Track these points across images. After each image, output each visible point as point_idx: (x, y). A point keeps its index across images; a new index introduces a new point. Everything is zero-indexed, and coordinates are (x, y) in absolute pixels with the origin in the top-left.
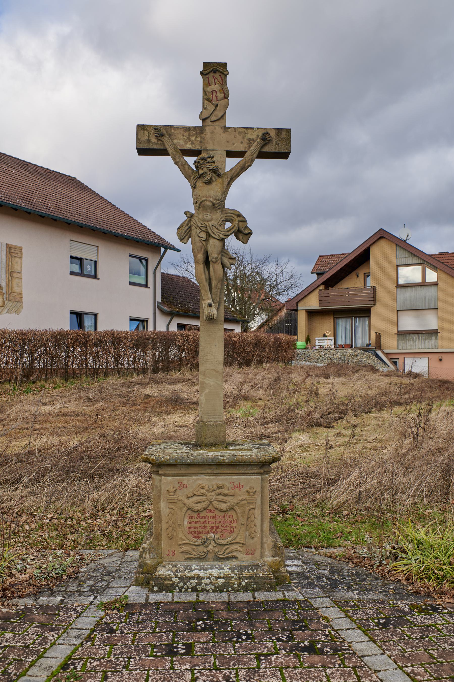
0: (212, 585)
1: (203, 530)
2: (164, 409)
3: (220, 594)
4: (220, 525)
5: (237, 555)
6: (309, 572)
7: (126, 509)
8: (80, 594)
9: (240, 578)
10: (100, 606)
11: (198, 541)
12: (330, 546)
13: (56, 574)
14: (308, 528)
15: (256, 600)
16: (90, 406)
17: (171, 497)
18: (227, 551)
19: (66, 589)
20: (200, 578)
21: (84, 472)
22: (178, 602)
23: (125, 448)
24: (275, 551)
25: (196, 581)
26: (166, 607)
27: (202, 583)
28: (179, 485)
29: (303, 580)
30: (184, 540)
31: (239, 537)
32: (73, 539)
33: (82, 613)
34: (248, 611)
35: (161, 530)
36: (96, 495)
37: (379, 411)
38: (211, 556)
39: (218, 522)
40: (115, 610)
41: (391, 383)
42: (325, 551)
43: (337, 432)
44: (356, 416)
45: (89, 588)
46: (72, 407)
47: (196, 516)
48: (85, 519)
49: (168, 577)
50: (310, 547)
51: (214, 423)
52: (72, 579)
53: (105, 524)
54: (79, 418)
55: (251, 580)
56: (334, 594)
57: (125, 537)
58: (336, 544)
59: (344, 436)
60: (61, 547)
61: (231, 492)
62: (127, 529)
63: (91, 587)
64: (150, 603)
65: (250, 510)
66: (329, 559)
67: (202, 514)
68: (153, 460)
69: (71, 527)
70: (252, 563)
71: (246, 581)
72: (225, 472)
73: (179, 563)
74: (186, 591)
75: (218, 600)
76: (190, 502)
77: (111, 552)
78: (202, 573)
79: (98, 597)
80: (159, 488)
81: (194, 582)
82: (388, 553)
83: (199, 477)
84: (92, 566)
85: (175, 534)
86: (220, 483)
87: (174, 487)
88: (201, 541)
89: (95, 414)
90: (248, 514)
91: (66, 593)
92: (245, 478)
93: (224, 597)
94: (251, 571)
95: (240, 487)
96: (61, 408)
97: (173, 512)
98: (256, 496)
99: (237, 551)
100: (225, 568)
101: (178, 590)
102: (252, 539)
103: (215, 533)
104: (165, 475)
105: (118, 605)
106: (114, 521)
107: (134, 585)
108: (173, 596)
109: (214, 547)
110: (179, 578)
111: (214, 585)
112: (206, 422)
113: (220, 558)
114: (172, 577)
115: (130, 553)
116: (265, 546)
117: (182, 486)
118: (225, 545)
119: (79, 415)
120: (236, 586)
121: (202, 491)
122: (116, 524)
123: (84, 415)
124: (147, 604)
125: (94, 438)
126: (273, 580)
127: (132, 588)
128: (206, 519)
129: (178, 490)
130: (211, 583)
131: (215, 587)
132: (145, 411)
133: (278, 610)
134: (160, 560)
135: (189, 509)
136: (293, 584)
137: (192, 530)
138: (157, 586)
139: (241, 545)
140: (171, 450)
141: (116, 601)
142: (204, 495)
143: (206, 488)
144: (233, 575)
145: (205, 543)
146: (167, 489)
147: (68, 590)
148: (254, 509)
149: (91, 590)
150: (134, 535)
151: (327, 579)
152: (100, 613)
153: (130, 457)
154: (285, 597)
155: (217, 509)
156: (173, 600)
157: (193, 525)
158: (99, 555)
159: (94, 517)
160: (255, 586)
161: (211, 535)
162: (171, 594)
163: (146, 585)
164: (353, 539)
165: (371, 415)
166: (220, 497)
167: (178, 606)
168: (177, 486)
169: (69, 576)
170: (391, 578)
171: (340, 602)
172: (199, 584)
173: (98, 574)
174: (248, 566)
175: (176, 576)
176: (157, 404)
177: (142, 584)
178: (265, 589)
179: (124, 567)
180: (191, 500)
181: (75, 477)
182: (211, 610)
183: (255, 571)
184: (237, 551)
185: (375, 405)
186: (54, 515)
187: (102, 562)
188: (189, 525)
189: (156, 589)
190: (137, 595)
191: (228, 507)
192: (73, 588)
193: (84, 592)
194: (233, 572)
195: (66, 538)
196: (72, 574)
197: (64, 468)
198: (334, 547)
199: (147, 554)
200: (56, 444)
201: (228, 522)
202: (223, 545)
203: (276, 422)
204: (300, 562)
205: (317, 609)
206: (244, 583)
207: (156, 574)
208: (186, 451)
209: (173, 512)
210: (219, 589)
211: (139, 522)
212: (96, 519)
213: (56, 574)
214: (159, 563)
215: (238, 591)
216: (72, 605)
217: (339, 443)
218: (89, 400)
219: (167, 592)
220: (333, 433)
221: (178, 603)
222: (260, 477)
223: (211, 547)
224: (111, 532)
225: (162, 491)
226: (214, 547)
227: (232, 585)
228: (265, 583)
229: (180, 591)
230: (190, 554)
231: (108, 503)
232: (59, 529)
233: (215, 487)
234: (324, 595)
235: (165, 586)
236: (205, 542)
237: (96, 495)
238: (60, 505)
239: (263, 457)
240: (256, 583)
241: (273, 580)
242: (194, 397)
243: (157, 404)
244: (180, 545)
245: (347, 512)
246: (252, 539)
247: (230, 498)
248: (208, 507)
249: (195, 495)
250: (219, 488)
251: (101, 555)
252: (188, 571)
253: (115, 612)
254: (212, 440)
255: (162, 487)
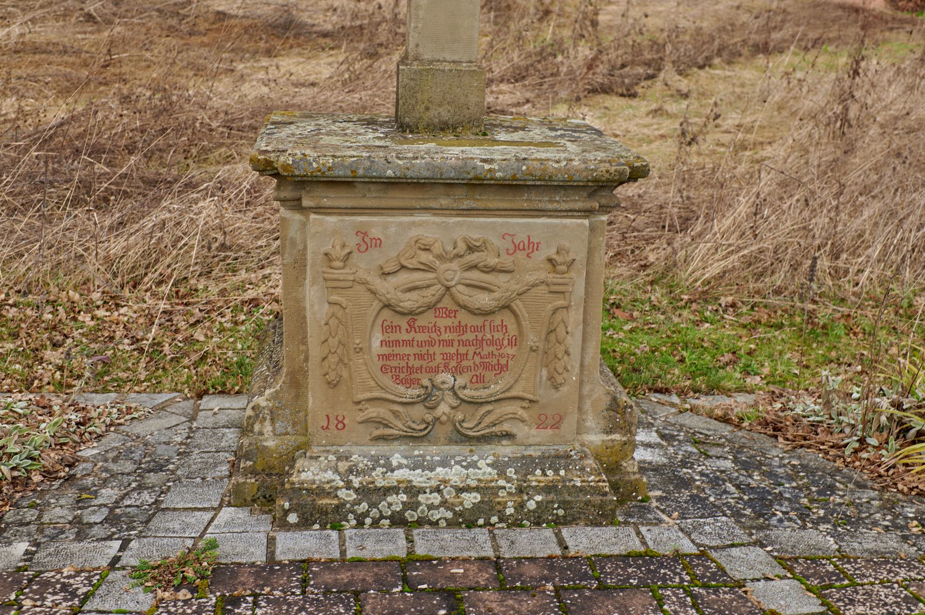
0: (447, 509)
1: (424, 364)
2: (262, 44)
3: (469, 534)
4: (472, 350)
5: (514, 431)
6: (684, 464)
7: (193, 281)
8: (82, 530)
9: (520, 491)
10: (140, 573)
11: (410, 391)
12: (713, 389)
13: (13, 469)
14: (647, 337)
15: (572, 553)
16: (91, 33)
17: (337, 274)
18: (488, 420)
19: (40, 517)
20: (413, 491)
21: (86, 186)
22: (360, 561)
23: (179, 130)
24: (611, 419)
25: (404, 497)
26: (328, 577)
27: (419, 504)
28: (358, 240)
29: (678, 487)
30: (370, 390)
31: (522, 383)
32: (60, 362)
33: (87, 597)
34: (557, 590)
35: (306, 359)
36: (116, 246)
37: (729, 63)
38: (442, 431)
39: (464, 343)
40: (184, 591)
41: (738, 8)
42: (704, 402)
43: (654, 106)
44: (680, 73)
45: (105, 512)
46: (48, 32)
47: (405, 326)
48: (90, 307)
49: (327, 486)
50: (665, 391)
51: (453, 67)
52: (56, 484)
53: (141, 320)
54: (66, 58)
55: (552, 496)
56: (773, 533)
57: (195, 357)
58: (729, 384)
59: (669, 115)
60: (28, 384)
61: (507, 261)
62: (199, 335)
63: (112, 510)
64: (279, 563)
65: (555, 311)
66: (722, 425)
67: (421, 321)
68: (286, 167)
69: (54, 328)
70: (552, 450)
71: (539, 498)
72: (491, 205)
73: (355, 449)
74: (375, 524)
75: (466, 554)
76: (388, 287)
77: (161, 398)
78: (418, 478)
79: (134, 544)
80: (300, 247)
81: (397, 501)
82: (883, 419)
83: (418, 218)
84: (113, 440)
85: (345, 374)
86: (475, 235)
87: (344, 246)
88: (417, 392)
89: (105, 51)
90: (550, 323)
91: (40, 531)
92: (543, 224)
93: (480, 543)
94: (550, 473)
95: (531, 247)
96: (22, 35)
97: (340, 314)
98: (573, 274)
99: (516, 419)
100: (481, 463)
101: (354, 522)
102: (556, 388)
103: (458, 371)
104: (318, 210)
105: (190, 574)
106: (164, 312)
107: (229, 505)
108: (342, 543)
109: (453, 408)
110: (356, 490)
111: (452, 510)
112: (431, 62)
113: (466, 436)
114: (337, 488)
115: (212, 403)
116: (588, 405)
117: (368, 242)
118: (482, 403)
119: (66, 52)
120: (510, 511)
121: (425, 257)
122: (170, 320)
123: (77, 53)
124: (271, 568)
125: (104, 104)
126: (609, 497)
127: (227, 513)
128: (434, 335)
129: (356, 256)
130: (444, 503)
131: (455, 513)
132: (220, 48)
133: (637, 587)
134: (302, 439)
135: (387, 306)
136: (655, 504)
137: (394, 363)
138: (296, 511)
139: (525, 404)
140: (334, 140)
141: (183, 562)
142: (428, 268)
143: (437, 249)
144: (502, 483)
145: (428, 399)
146: (324, 249)
147: (46, 518)
148: (566, 308)
149: (112, 519)
150: (218, 352)
151: (738, 487)
152: (141, 597)
153: (194, 151)
154: (644, 543)
155: (465, 307)
156: (343, 553)
157: (397, 350)
158: (129, 408)
159: (113, 301)
160: (561, 512)
161: (445, 378)
162: (334, 534)
163: (263, 505)
164: (766, 371)
165: (712, 71)
166: (475, 276)
167: (361, 574)
168: (353, 242)
169: (49, 474)
170: (900, 486)
171: (796, 559)
172: (413, 505)
173: (129, 467)
174: (543, 458)
175: (349, 486)
176: (246, 32)
177: (254, 501)
178: (587, 518)
179: (198, 446)
180: (393, 280)
181: (61, 197)
182: (452, 586)
183: (562, 473)
184: (516, 419)
185: (719, 50)
186: (7, 295)
187: (138, 429)
188: (386, 350)
189: (293, 518)
190: (242, 537)
191: (494, 303)
192: (59, 512)
193: (91, 525)
194: (502, 474)
195: (41, 361)
196: (58, 467)
197: (30, 176)
198: (727, 392)
199: (268, 423)
200: (13, 116)
201: (492, 342)
202: (475, 403)
203: (517, 81)
204: (655, 434)
205: (741, 584)
206: (531, 505)
207: (294, 479)
208: (378, 143)
209: (340, 314)
210: (465, 520)
211: (228, 317)
212: (117, 305)
213: (13, 469)
214: (303, 448)
215: (516, 524)
216: (59, 571)
217: (662, 132)
218: (90, 18)
219: (323, 527)
220: (644, 110)
221: (359, 562)
222: (586, 222)
223: (443, 408)
224: (159, 344)
225: (309, 256)
226: (453, 408)
227: (499, 507)
228: (587, 503)
229: (360, 524)
230: (386, 426)
231: (147, 267)
232: (23, 334)
233: (462, 247)
234: (746, 539)
235: (318, 513)
236: (429, 395)
237: (116, 246)
238: (23, 269)
239: (604, 167)
240: (564, 504)
241: (609, 497)
242: (325, 21)
243: (246, 32)
244: (359, 403)
245: (730, 299)
246: (556, 388)
247: (501, 279)
248: (439, 301)
249: (403, 267)
250: (471, 249)
251: (136, 410)
252: (380, 470)
253: (184, 594)
254: (444, 113)
255: (310, 245)
